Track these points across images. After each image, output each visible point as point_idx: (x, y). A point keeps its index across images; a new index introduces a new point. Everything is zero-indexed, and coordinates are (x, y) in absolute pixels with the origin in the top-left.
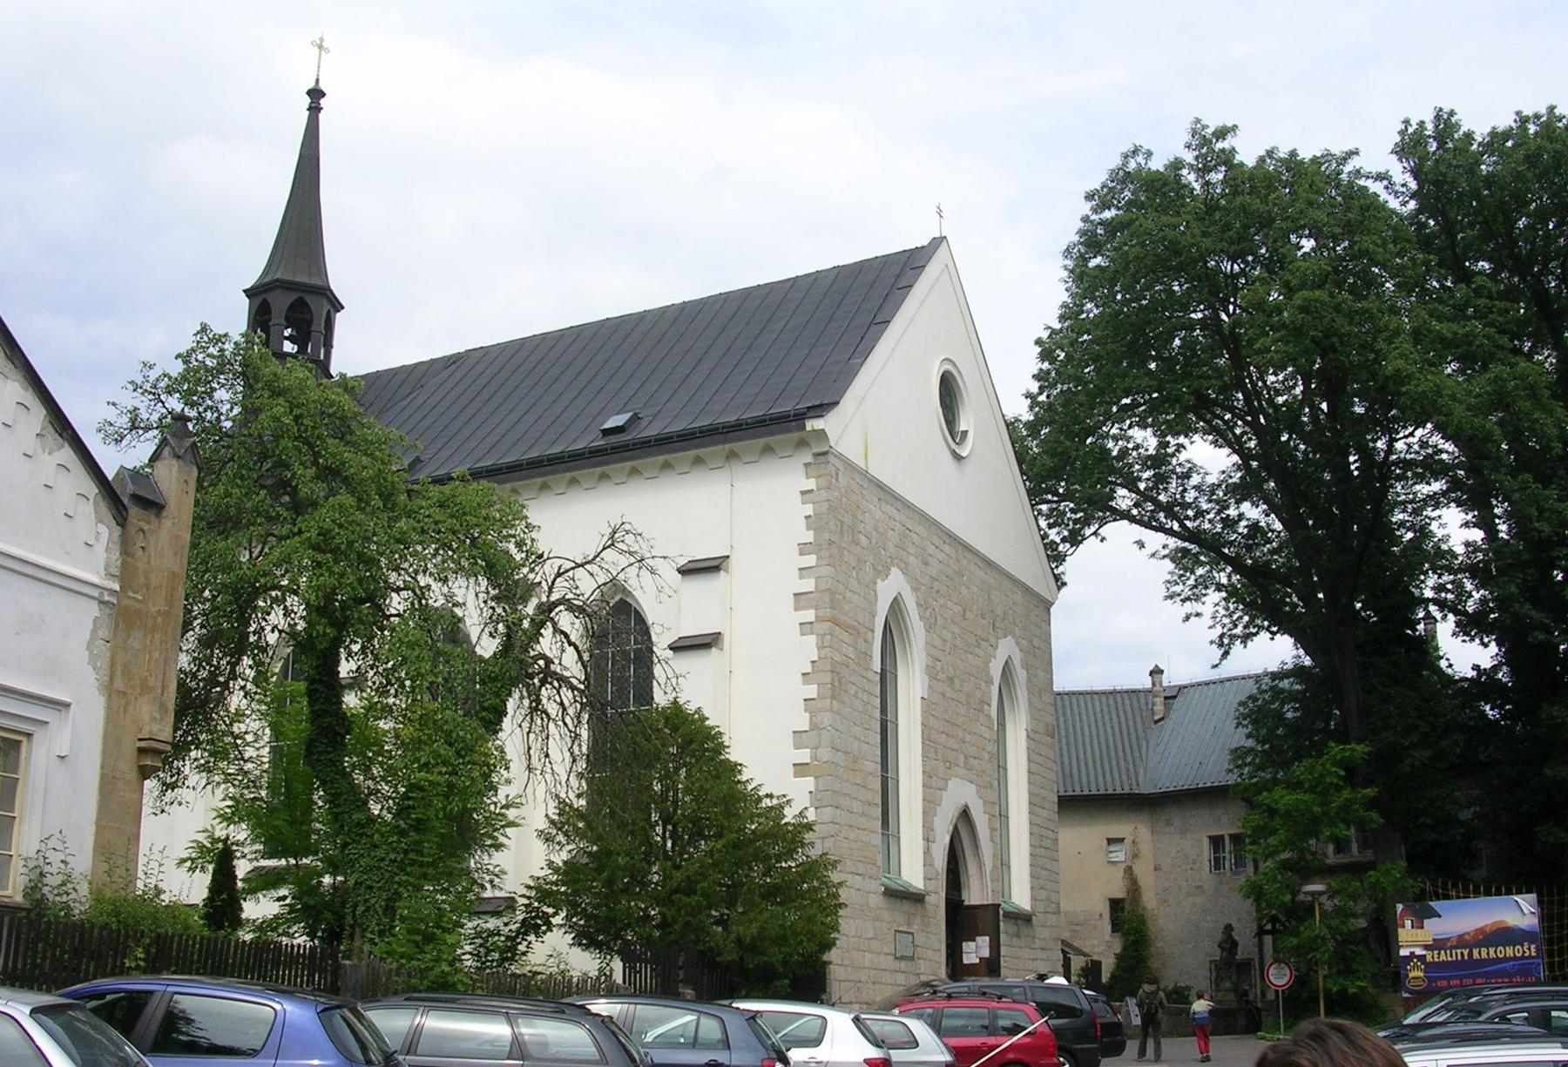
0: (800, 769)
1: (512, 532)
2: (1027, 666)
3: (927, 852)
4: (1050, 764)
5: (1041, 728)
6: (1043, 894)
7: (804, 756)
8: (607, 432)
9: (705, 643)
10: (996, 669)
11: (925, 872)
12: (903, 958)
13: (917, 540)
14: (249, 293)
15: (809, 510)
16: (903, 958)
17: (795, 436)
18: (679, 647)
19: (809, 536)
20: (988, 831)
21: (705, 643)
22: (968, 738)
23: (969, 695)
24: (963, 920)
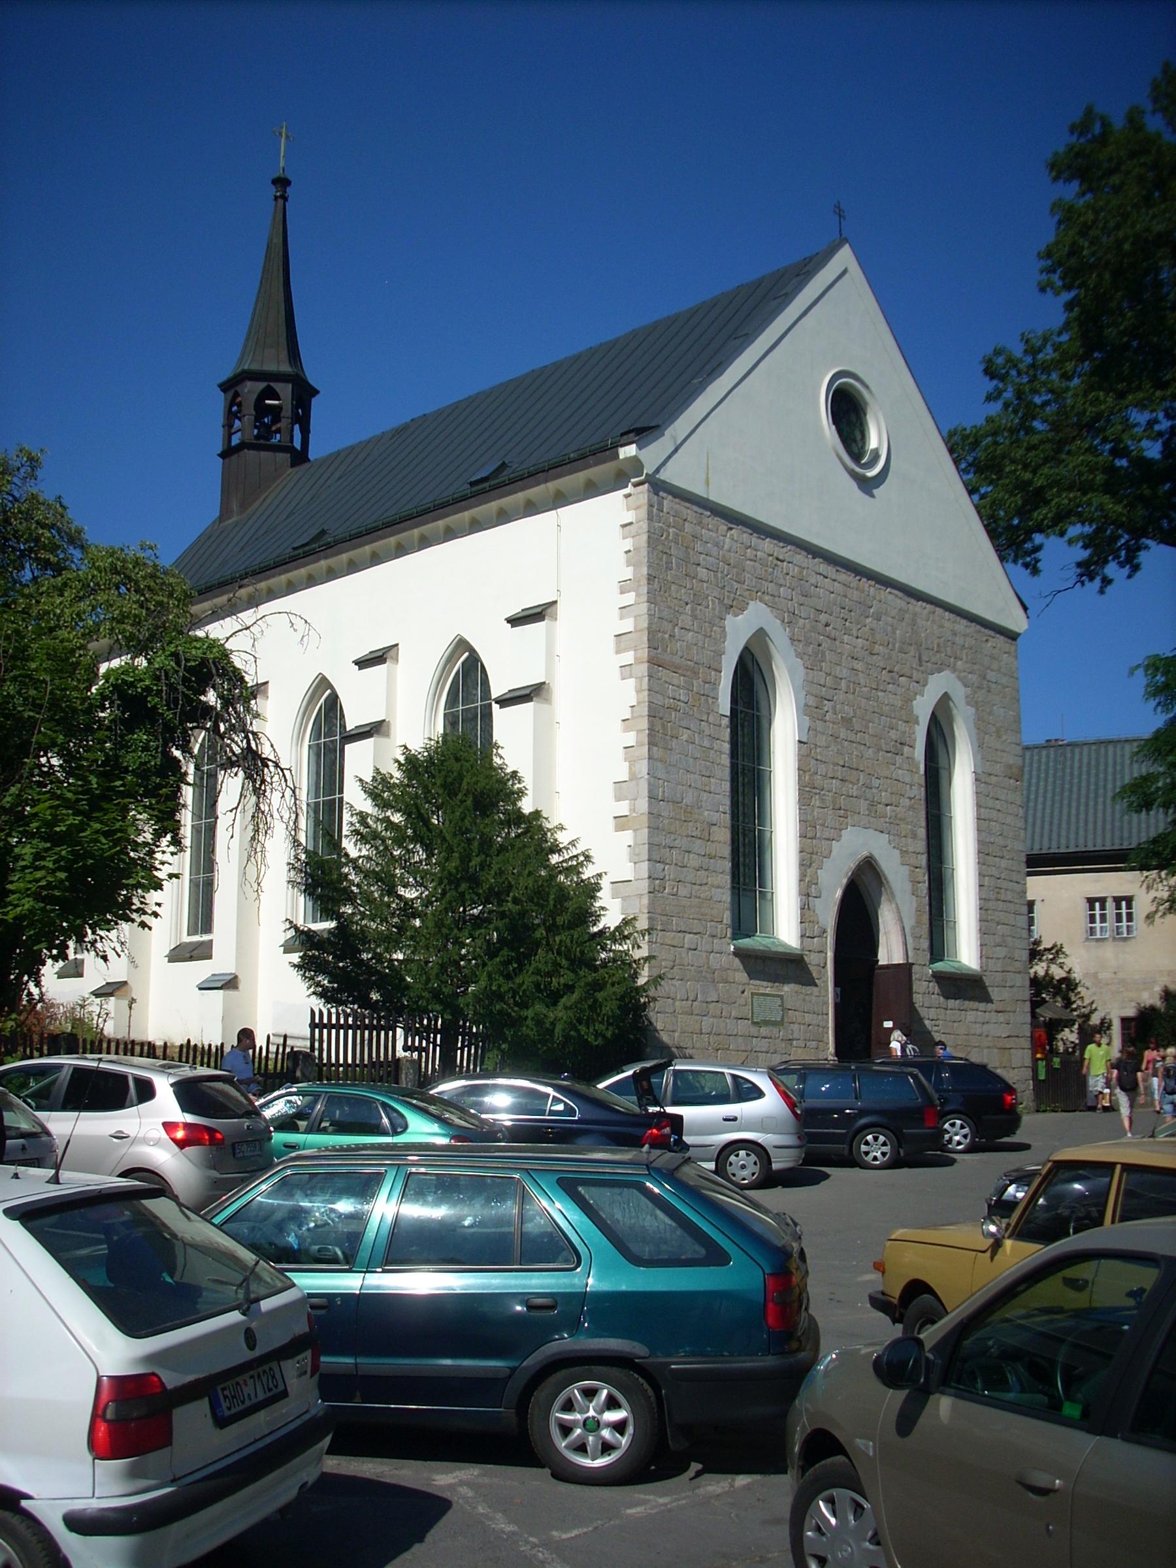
0: (621, 823)
2: (971, 701)
5: (998, 769)
6: (1001, 952)
7: (623, 808)
10: (923, 707)
12: (766, 1023)
14: (225, 387)
15: (628, 544)
16: (766, 1023)
18: (504, 702)
20: (908, 886)
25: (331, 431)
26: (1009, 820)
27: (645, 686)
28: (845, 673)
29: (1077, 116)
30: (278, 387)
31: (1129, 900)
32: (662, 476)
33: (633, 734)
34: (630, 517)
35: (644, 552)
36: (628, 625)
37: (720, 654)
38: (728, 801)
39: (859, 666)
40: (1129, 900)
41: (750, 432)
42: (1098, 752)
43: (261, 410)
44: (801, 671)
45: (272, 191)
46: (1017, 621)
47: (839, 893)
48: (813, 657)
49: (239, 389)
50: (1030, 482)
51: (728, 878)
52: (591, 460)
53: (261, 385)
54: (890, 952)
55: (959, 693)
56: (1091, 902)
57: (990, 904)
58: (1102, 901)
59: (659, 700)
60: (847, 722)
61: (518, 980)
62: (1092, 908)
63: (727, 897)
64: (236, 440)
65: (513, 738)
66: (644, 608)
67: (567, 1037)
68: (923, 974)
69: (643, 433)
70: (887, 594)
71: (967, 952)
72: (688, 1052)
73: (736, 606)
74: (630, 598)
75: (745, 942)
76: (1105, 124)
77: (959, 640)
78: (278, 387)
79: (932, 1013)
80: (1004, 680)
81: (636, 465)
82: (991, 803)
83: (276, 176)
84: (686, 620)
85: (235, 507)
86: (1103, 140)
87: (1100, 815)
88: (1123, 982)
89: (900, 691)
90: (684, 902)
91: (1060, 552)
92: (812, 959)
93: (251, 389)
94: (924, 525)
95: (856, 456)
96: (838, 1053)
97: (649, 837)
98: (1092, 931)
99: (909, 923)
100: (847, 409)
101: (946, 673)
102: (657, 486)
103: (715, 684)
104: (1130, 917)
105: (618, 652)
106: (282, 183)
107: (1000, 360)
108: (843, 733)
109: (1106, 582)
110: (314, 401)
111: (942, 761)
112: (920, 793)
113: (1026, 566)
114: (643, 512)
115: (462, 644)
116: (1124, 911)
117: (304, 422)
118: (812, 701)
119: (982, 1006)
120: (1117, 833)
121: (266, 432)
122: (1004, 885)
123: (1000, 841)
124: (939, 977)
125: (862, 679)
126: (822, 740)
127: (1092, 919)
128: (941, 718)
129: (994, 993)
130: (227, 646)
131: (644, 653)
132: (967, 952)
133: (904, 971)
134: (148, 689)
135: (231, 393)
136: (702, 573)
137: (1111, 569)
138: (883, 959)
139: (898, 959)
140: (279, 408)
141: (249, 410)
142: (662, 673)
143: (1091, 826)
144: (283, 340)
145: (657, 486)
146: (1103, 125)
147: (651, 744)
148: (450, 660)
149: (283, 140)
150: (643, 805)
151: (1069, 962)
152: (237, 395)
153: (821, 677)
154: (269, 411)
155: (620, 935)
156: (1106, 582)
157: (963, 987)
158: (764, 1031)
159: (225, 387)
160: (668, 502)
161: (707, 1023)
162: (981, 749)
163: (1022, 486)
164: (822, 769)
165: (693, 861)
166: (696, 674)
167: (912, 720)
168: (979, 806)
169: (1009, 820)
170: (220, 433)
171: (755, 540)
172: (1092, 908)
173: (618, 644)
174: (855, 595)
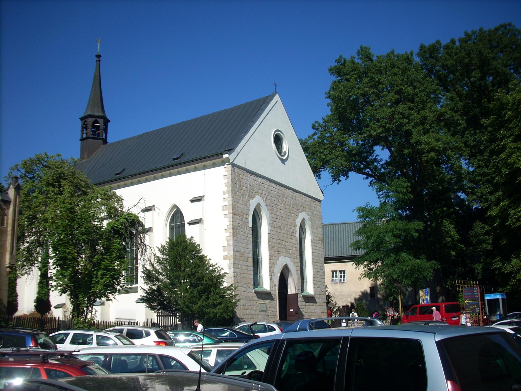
0: (225, 257)
1: (511, 138)
2: (310, 220)
3: (271, 279)
4: (321, 249)
5: (317, 238)
6: (319, 289)
7: (226, 253)
8: (116, 174)
9: (197, 222)
10: (298, 222)
11: (271, 285)
12: (262, 311)
13: (266, 186)
14: (82, 119)
15: (226, 181)
16: (262, 311)
17: (219, 160)
18: (190, 224)
19: (226, 189)
20: (296, 272)
21: (197, 222)
22: (287, 244)
23: (287, 231)
24: (285, 300)
25: (114, 135)
26: (320, 252)
27: (231, 220)
28: (279, 214)
29: (338, 58)
30: (98, 120)
31: (344, 271)
32: (234, 162)
33: (228, 233)
34: (226, 173)
35: (230, 183)
36: (226, 203)
37: (249, 210)
38: (252, 251)
39: (282, 212)
40: (344, 271)
41: (255, 149)
42: (333, 227)
43: (93, 126)
44: (269, 214)
45: (95, 59)
46: (321, 197)
47: (279, 275)
48: (271, 211)
49: (86, 120)
50: (325, 159)
51: (252, 272)
52: (215, 157)
53: (94, 119)
54: (292, 290)
55: (307, 218)
56: (333, 272)
57: (316, 276)
58: (336, 271)
59: (235, 224)
60: (280, 227)
61: (208, 302)
62: (333, 274)
63: (252, 277)
64: (85, 136)
65: (190, 232)
66: (231, 199)
67: (221, 316)
68: (300, 296)
69: (230, 151)
70: (289, 191)
71: (310, 290)
72: (244, 320)
73: (252, 197)
74: (226, 196)
75: (256, 289)
76: (345, 61)
77: (307, 203)
78: (98, 120)
79: (302, 307)
80: (318, 214)
81: (228, 159)
82: (315, 248)
83: (97, 54)
84: (241, 202)
85: (85, 156)
86: (344, 65)
87: (335, 246)
88: (342, 295)
89: (292, 218)
90: (242, 279)
91: (326, 174)
92: (273, 293)
93: (90, 121)
94: (297, 172)
95: (280, 153)
96: (280, 319)
97: (234, 261)
98: (333, 280)
99: (296, 282)
100: (278, 140)
101: (304, 212)
102: (233, 165)
103: (248, 219)
104: (344, 276)
105: (223, 210)
106: (99, 56)
107: (317, 125)
108: (279, 231)
109: (340, 181)
110: (109, 124)
111: (303, 237)
112: (298, 246)
113: (317, 176)
114: (230, 172)
115: (175, 206)
116: (342, 274)
117: (106, 130)
118: (271, 222)
119: (314, 304)
120: (340, 252)
121: (94, 133)
122: (319, 270)
123: (318, 258)
124: (256, 293)
125: (283, 215)
126: (274, 233)
127: (333, 277)
128: (302, 225)
129: (317, 301)
130: (139, 216)
131: (231, 211)
132: (310, 290)
133: (296, 295)
134: (120, 228)
135: (83, 121)
136: (244, 188)
137: (341, 178)
138: (290, 292)
139: (294, 292)
140: (99, 126)
141: (90, 126)
142: (235, 216)
143: (332, 249)
144: (100, 105)
145: (233, 165)
146: (344, 61)
147: (233, 236)
148: (171, 211)
149: (99, 43)
150: (232, 253)
151: (329, 290)
152: (85, 122)
153: (273, 215)
154: (95, 128)
155: (229, 288)
156: (340, 181)
157: (310, 299)
158: (262, 313)
159: (82, 119)
160: (236, 169)
161: (248, 311)
162: (312, 232)
163: (323, 160)
164: (274, 241)
165: (244, 267)
166: (243, 216)
167: (295, 226)
168: (312, 249)
169: (320, 252)
170: (80, 133)
171: (257, 178)
172: (333, 274)
173: (223, 208)
174: (281, 192)
